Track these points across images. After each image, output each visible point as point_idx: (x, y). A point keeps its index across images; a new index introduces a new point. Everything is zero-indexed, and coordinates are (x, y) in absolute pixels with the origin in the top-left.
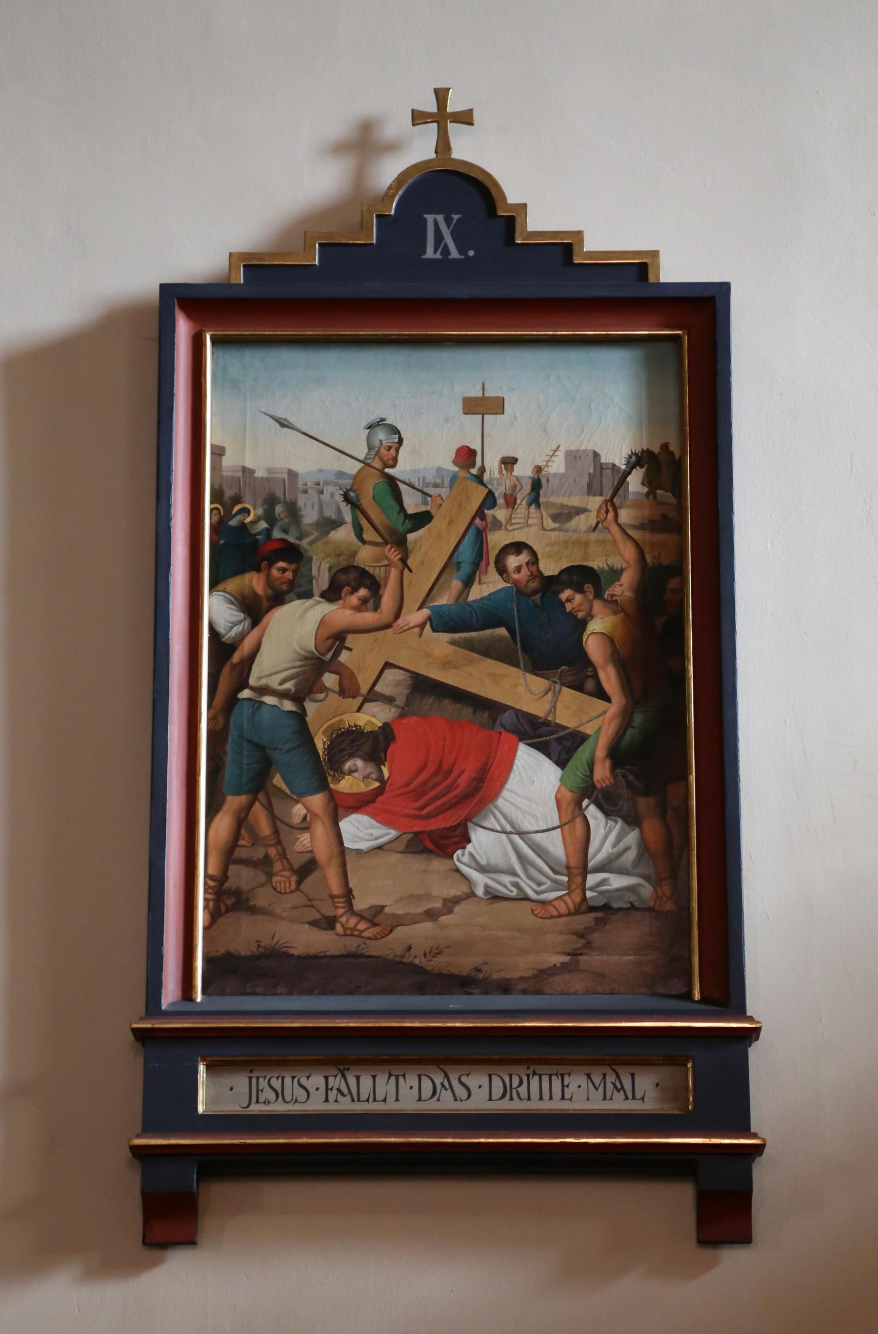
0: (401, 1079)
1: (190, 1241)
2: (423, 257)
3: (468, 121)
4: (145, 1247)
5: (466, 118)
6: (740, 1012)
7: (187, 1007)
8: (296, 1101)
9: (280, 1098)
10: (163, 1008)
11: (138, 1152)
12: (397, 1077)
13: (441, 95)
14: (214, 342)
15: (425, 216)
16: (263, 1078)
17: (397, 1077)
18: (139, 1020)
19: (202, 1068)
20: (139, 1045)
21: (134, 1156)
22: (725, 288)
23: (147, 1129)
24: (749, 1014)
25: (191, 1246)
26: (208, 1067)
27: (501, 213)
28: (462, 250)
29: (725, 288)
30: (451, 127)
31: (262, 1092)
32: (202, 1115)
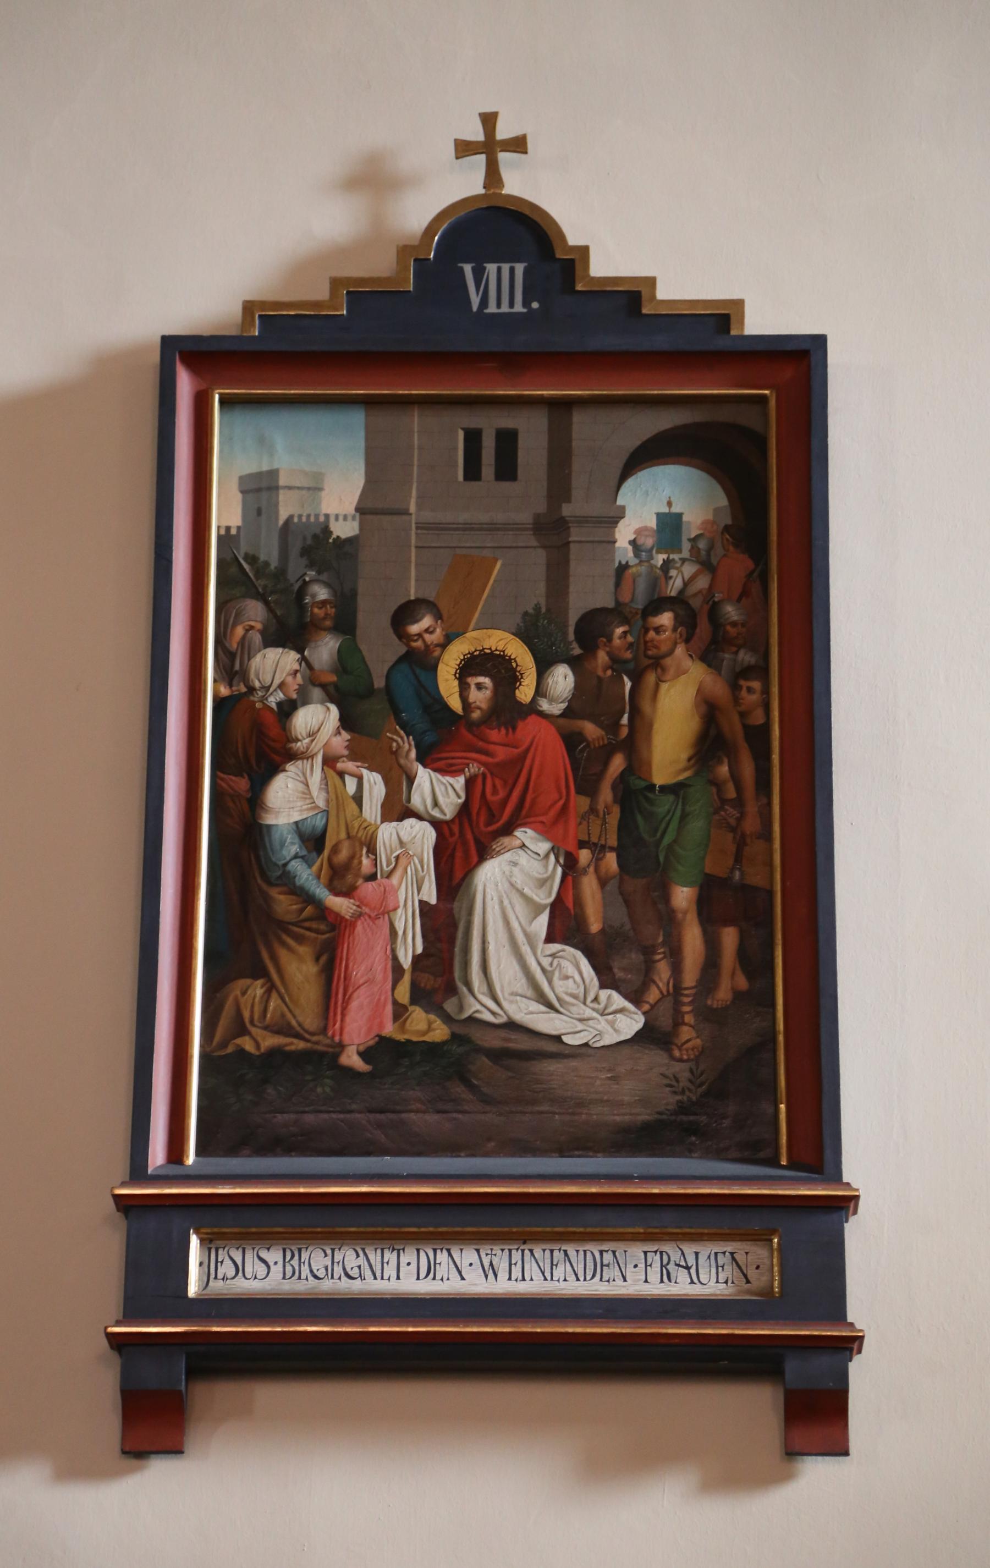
0: (401, 1251)
1: (176, 1450)
2: (474, 265)
3: (524, 151)
4: (123, 1455)
5: (519, 145)
6: (836, 1177)
7: (175, 1170)
8: (256, 1278)
9: (240, 1274)
10: (149, 1172)
11: (117, 1342)
12: (399, 1251)
13: (489, 120)
14: (222, 402)
15: (460, 265)
16: (222, 1249)
17: (399, 1251)
18: (120, 1185)
19: (194, 1241)
20: (119, 1216)
21: (112, 1347)
22: (820, 341)
23: (129, 1316)
24: (845, 1180)
25: (179, 1456)
26: (206, 1242)
27: (559, 255)
28: (526, 303)
29: (820, 341)
30: (503, 157)
31: (221, 1265)
32: (193, 1300)
